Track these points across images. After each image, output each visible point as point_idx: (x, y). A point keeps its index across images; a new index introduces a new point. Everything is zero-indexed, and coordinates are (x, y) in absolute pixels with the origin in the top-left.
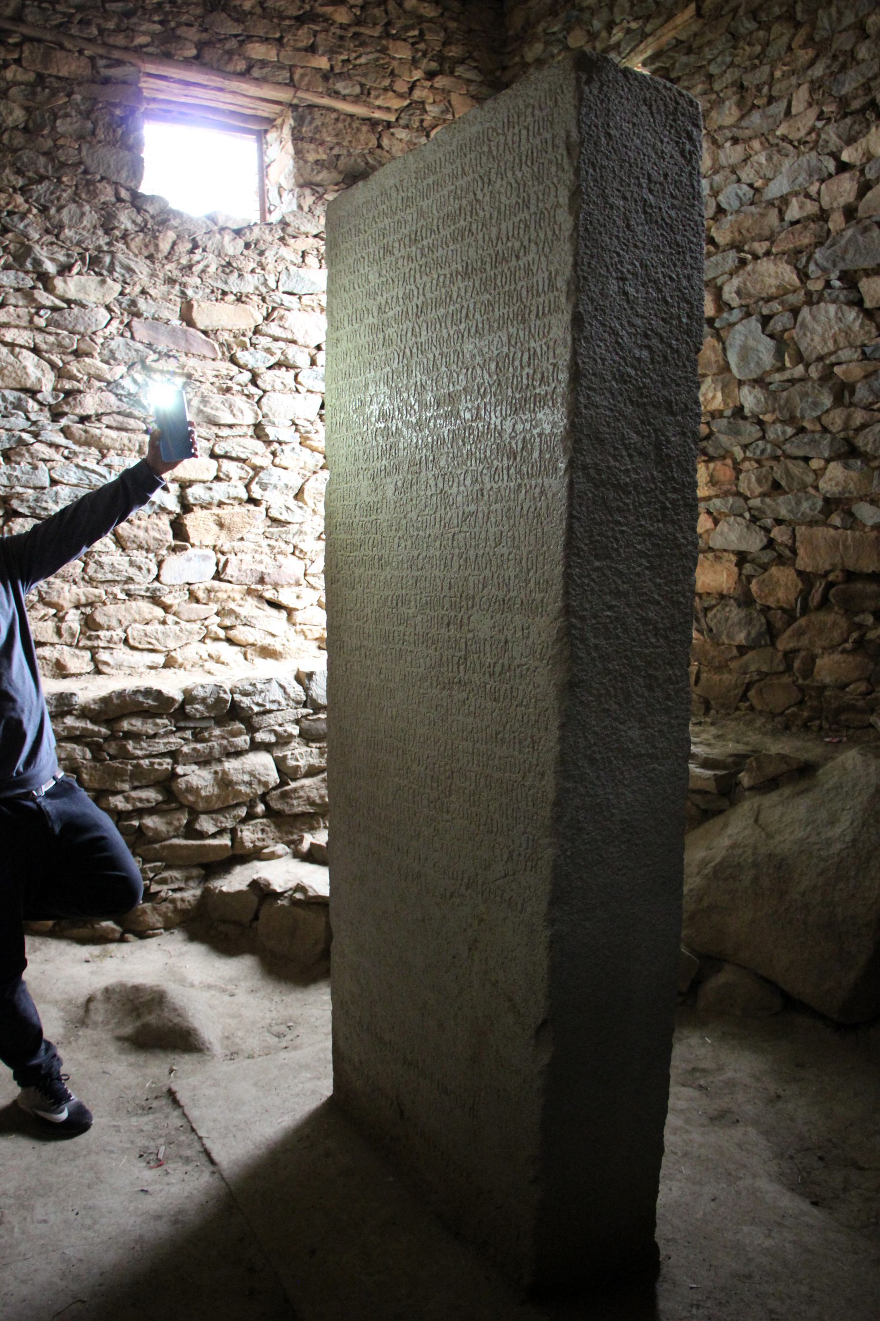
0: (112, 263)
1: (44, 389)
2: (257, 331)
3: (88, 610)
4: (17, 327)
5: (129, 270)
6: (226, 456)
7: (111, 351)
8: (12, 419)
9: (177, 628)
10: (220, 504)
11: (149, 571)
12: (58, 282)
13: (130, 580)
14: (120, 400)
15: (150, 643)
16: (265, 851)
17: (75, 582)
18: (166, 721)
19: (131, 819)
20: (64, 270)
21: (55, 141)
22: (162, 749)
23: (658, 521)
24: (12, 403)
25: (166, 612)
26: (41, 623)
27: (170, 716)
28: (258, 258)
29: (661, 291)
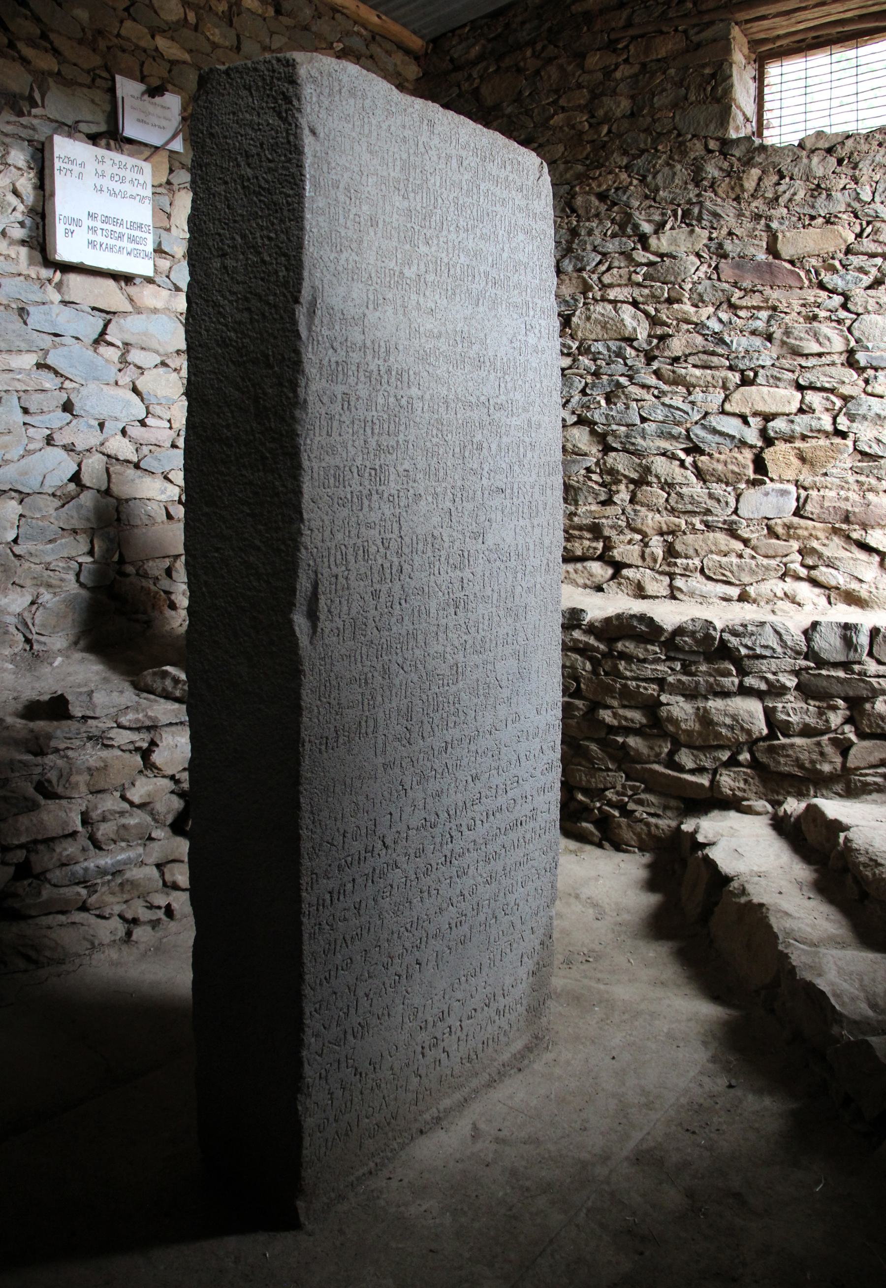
0: (700, 212)
1: (639, 337)
2: (848, 251)
3: (670, 538)
4: (619, 285)
5: (716, 215)
6: (812, 387)
7: (700, 295)
8: (613, 366)
9: (753, 562)
10: (804, 438)
11: (727, 503)
12: (653, 242)
13: (708, 512)
14: (706, 340)
15: (724, 575)
16: (745, 803)
17: (659, 512)
18: (657, 649)
19: (617, 734)
20: (660, 227)
21: (652, 117)
22: (649, 674)
23: (259, 470)
24: (614, 352)
25: (746, 546)
26: (628, 547)
27: (662, 645)
28: (850, 172)
29: (259, 253)
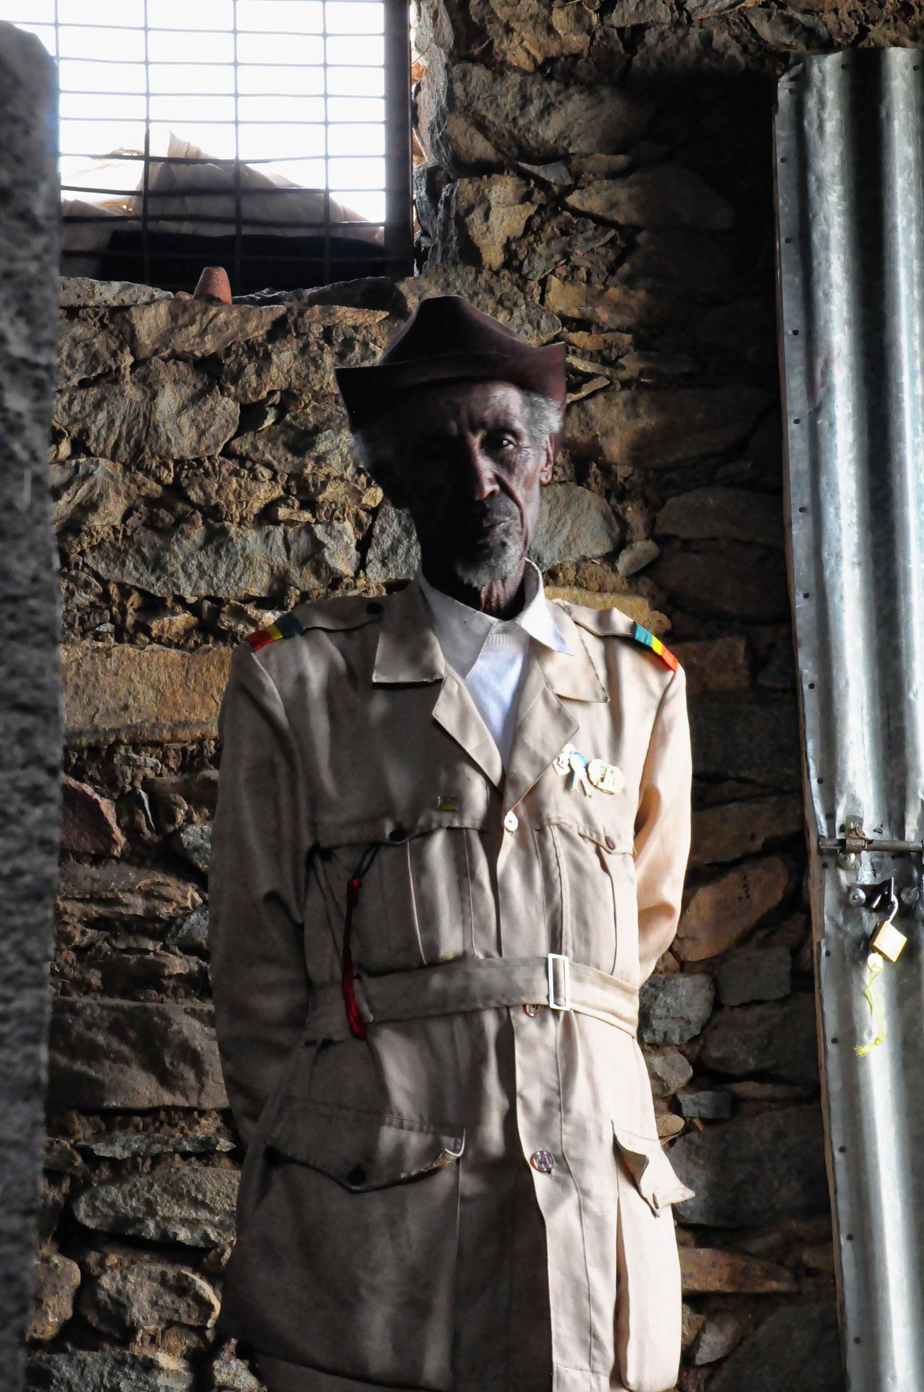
6: (124, 1237)
28: (285, 462)
